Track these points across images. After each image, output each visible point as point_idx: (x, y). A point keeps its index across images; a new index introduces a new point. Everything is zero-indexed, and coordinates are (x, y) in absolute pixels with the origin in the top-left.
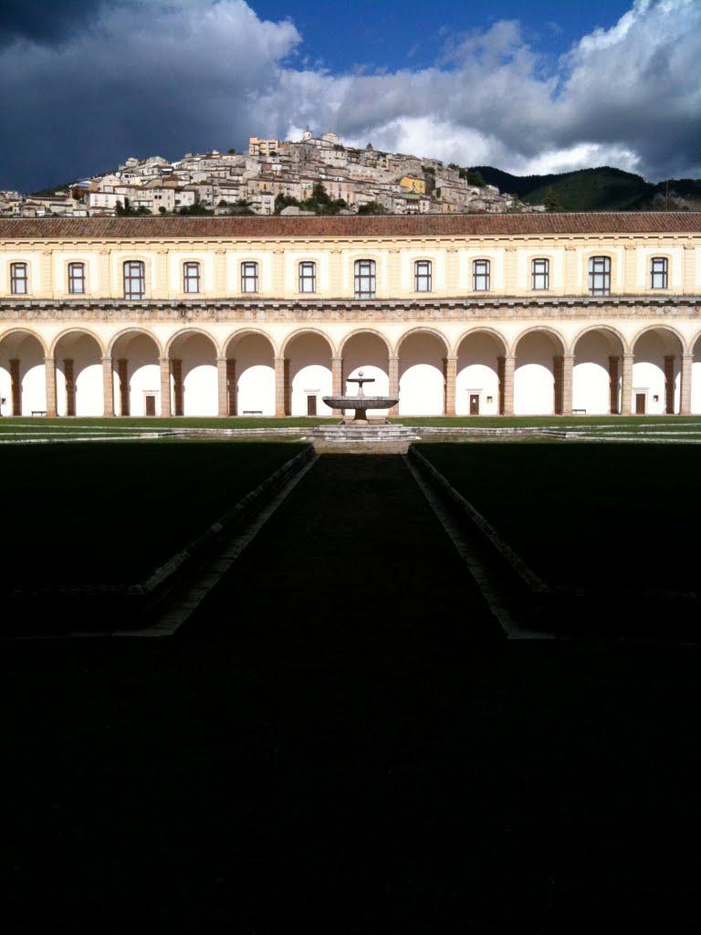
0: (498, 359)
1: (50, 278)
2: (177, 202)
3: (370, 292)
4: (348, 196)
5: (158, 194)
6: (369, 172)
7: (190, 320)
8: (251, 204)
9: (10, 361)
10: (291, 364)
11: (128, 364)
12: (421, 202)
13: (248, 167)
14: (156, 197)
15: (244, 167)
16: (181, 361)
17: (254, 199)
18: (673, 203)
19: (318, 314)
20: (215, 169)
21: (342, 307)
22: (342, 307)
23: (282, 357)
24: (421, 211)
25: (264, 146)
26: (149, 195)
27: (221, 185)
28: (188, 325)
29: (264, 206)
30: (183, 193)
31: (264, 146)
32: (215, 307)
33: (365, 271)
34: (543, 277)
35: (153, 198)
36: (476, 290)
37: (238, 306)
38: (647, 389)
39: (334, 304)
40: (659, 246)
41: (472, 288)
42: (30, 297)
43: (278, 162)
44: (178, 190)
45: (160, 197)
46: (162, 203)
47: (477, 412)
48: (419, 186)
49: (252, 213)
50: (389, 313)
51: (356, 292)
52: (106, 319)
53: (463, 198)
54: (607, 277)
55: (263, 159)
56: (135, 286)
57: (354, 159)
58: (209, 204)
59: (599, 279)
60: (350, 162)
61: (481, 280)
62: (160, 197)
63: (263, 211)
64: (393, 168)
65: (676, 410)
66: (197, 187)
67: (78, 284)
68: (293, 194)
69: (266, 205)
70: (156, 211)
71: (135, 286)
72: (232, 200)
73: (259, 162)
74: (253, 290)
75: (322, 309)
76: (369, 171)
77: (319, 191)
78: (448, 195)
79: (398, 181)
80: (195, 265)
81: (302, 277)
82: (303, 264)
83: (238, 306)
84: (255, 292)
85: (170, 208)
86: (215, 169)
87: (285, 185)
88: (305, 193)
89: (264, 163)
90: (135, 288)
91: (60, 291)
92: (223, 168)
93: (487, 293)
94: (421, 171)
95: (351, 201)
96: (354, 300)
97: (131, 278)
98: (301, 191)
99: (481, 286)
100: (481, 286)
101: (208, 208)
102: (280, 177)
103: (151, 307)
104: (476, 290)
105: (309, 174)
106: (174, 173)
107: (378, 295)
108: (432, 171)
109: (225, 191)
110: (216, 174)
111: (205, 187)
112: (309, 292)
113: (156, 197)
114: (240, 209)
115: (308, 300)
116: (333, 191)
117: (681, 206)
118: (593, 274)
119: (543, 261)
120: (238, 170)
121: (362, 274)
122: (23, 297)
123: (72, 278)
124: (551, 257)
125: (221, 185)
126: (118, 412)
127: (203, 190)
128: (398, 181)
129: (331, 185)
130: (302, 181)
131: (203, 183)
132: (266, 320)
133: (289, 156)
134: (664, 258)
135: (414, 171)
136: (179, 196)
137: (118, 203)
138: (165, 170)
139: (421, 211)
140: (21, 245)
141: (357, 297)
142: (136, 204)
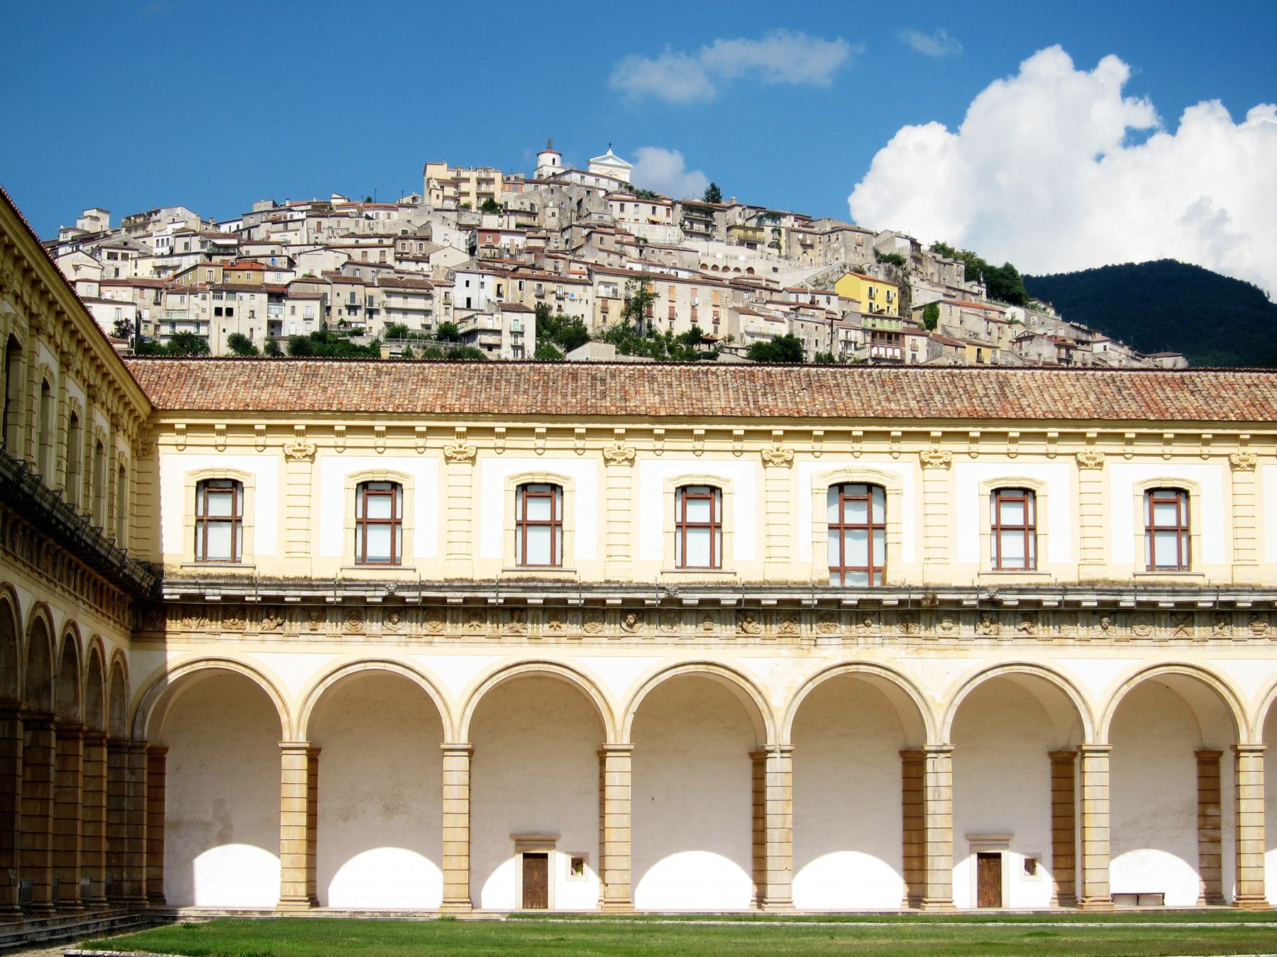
0: (752, 755)
2: (274, 325)
3: (870, 570)
4: (716, 322)
5: (224, 304)
6: (742, 258)
8: (472, 334)
9: (1051, 754)
10: (321, 758)
11: (168, 756)
12: (908, 339)
13: (437, 239)
14: (218, 311)
15: (427, 239)
16: (166, 750)
17: (484, 322)
18: (268, 349)
20: (352, 241)
21: (1113, 611)
22: (1113, 611)
23: (301, 738)
24: (908, 362)
25: (464, 187)
27: (384, 283)
29: (507, 340)
30: (289, 303)
31: (464, 187)
32: (921, 610)
35: (209, 315)
36: (1152, 567)
37: (988, 611)
41: (989, 565)
43: (513, 227)
44: (277, 295)
45: (230, 312)
47: (997, 900)
48: (886, 296)
49: (477, 358)
51: (832, 570)
53: (995, 334)
55: (467, 219)
56: (379, 542)
57: (699, 227)
58: (359, 333)
60: (691, 234)
61: (539, 540)
62: (230, 312)
63: (507, 353)
64: (800, 250)
65: (1231, 893)
66: (324, 288)
70: (219, 345)
71: (379, 542)
73: (462, 227)
74: (227, 554)
76: (743, 257)
78: (956, 322)
81: (684, 527)
83: (988, 611)
84: (1180, 566)
86: (352, 241)
87: (553, 287)
88: (605, 311)
92: (375, 241)
94: (873, 260)
95: (723, 332)
96: (827, 590)
101: (358, 341)
102: (533, 267)
106: (244, 249)
107: (893, 578)
108: (897, 261)
109: (397, 302)
110: (357, 255)
111: (345, 290)
112: (1170, 568)
113: (218, 311)
114: (446, 347)
115: (1021, 590)
117: (315, 350)
118: (840, 529)
119: (1172, 496)
120: (413, 247)
125: (384, 283)
127: (339, 296)
129: (671, 290)
130: (597, 278)
131: (336, 278)
133: (532, 214)
135: (856, 260)
136: (277, 312)
138: (218, 242)
139: (908, 362)
141: (835, 582)
142: (165, 330)
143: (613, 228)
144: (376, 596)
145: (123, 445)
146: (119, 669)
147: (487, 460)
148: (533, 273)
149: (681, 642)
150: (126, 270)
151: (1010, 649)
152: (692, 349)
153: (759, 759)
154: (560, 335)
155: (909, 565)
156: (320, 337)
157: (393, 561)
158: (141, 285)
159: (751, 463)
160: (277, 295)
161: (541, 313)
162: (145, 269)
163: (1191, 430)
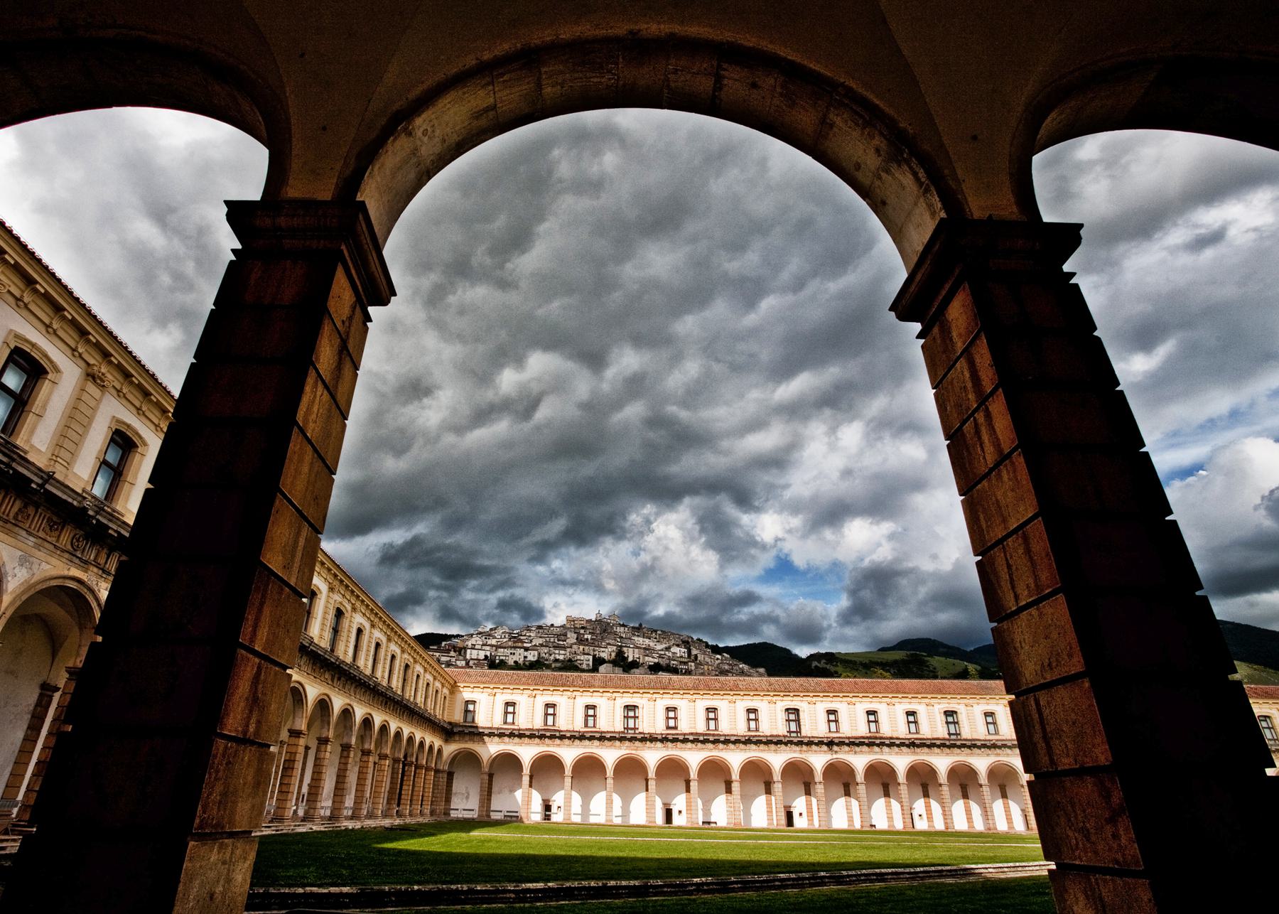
1: (733, 719)
3: (956, 734)
19: (926, 750)
21: (532, 735)
22: (532, 735)
26: (508, 651)
33: (631, 714)
39: (691, 738)
44: (526, 649)
46: (515, 658)
50: (976, 751)
52: (775, 751)
59: (951, 727)
67: (591, 721)
68: (603, 655)
69: (587, 661)
72: (561, 657)
75: (929, 746)
77: (620, 654)
79: (668, 649)
82: (749, 711)
85: (521, 661)
89: (578, 634)
90: (631, 725)
91: (579, 725)
98: (607, 652)
99: (873, 729)
100: (873, 729)
105: (612, 642)
116: (631, 655)
123: (506, 713)
126: (660, 819)
128: (668, 649)
131: (541, 645)
143: (615, 633)
144: (508, 732)
145: (446, 691)
146: (440, 751)
147: (858, 705)
148: (592, 644)
149: (585, 747)
150: (489, 642)
151: (753, 753)
152: (635, 664)
153: (647, 780)
154: (598, 662)
155: (725, 728)
156: (537, 661)
157: (675, 728)
158: (492, 646)
159: (485, 695)
160: (526, 649)
161: (594, 656)
162: (494, 642)
163: (796, 692)
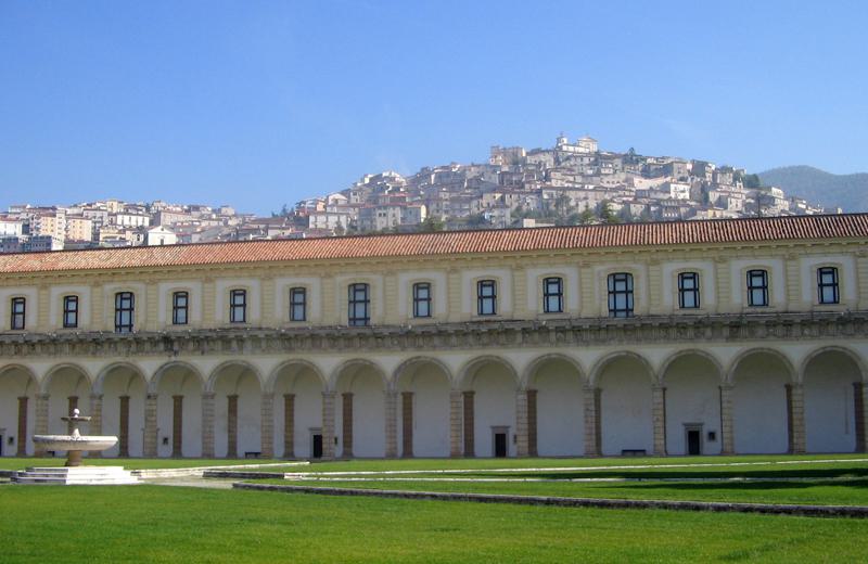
7: (176, 353)
9: (343, 395)
11: (354, 398)
14: (380, 215)
28: (173, 359)
34: (624, 295)
38: (508, 427)
40: (825, 254)
42: (500, 318)
54: (119, 307)
62: (385, 215)
80: (363, 287)
93: (493, 318)
97: (615, 292)
100: (239, 317)
103: (138, 341)
104: (482, 314)
121: (357, 299)
122: (240, 325)
124: (769, 267)
132: (253, 353)
134: (833, 269)
137: (338, 223)
140: (710, 252)
